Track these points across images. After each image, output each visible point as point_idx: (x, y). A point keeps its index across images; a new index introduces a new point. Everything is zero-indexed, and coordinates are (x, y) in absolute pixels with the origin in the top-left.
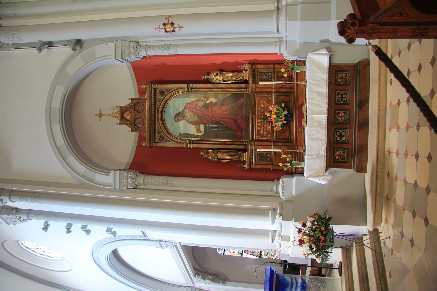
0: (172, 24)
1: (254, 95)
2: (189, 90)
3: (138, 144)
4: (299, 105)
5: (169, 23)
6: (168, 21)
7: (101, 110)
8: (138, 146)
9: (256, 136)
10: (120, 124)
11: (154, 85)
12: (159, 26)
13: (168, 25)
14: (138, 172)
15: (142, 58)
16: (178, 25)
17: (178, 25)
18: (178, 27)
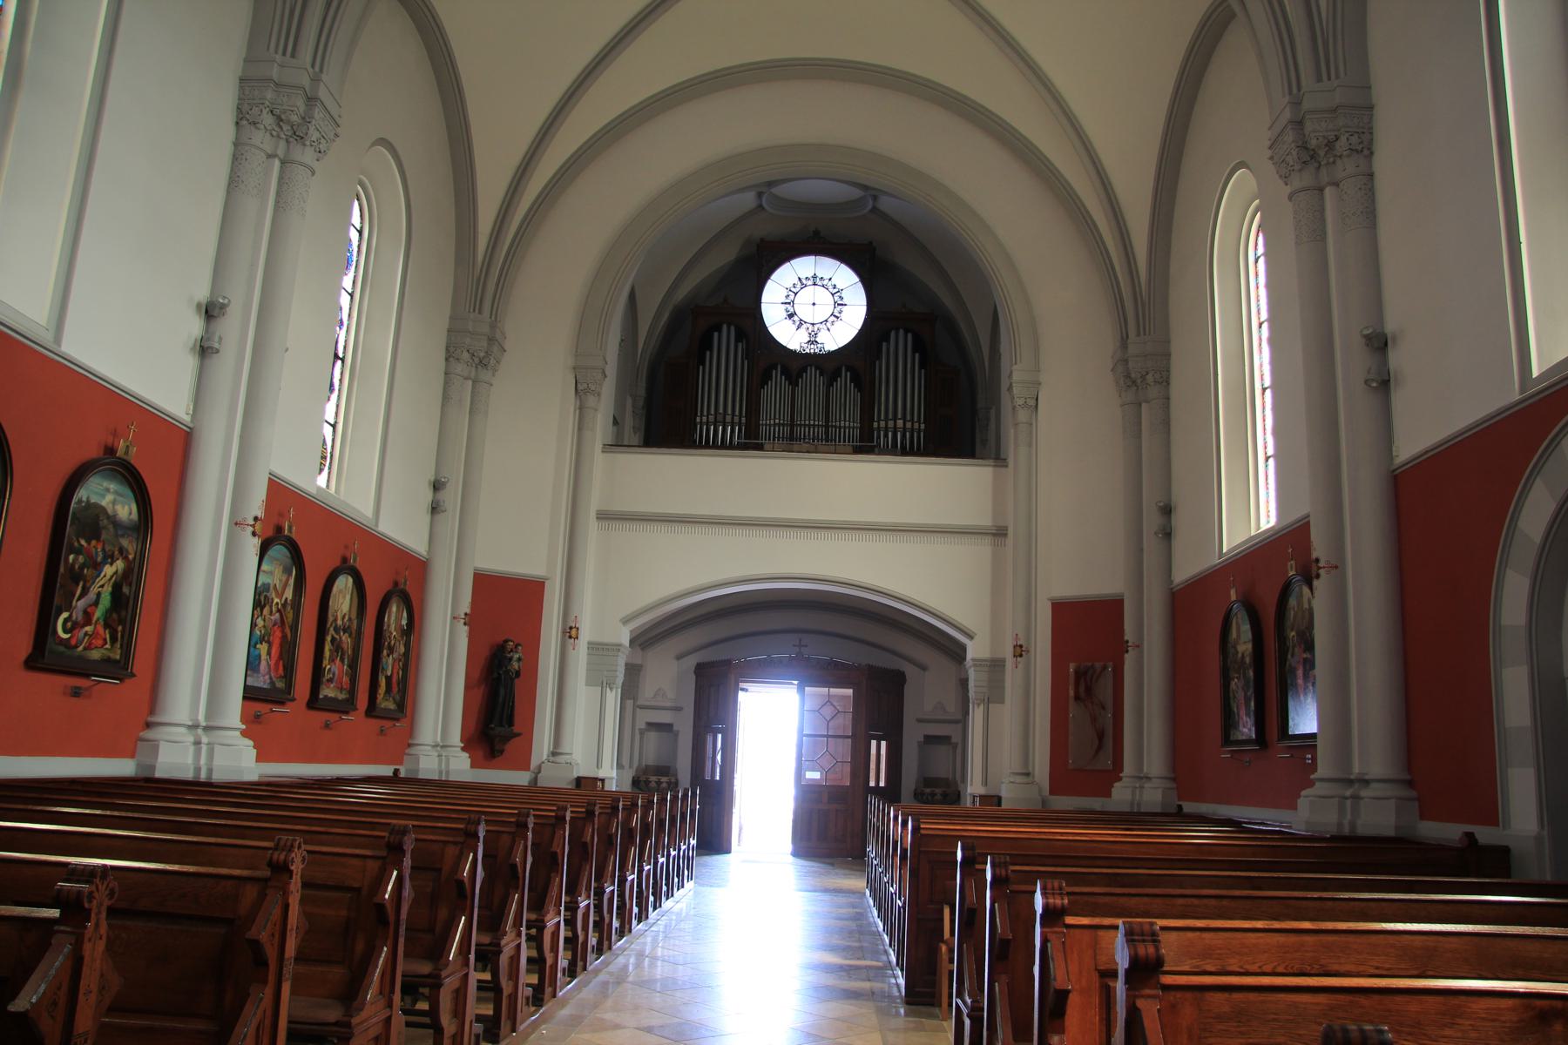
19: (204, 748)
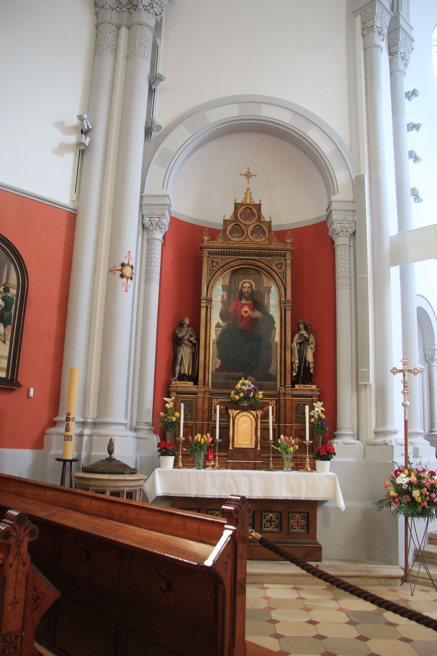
0: (123, 265)
1: (275, 396)
2: (283, 305)
3: (206, 229)
4: (257, 381)
5: (121, 269)
6: (119, 270)
7: (255, 177)
8: (203, 228)
9: (217, 399)
10: (235, 204)
11: (290, 254)
12: (123, 285)
13: (123, 271)
14: (166, 231)
15: (332, 238)
16: (125, 257)
17: (125, 257)
18: (128, 259)
19: (85, 439)
